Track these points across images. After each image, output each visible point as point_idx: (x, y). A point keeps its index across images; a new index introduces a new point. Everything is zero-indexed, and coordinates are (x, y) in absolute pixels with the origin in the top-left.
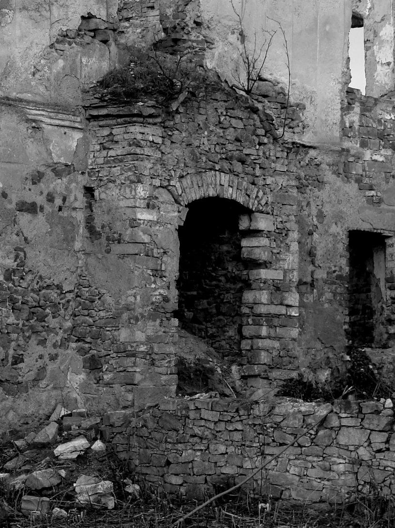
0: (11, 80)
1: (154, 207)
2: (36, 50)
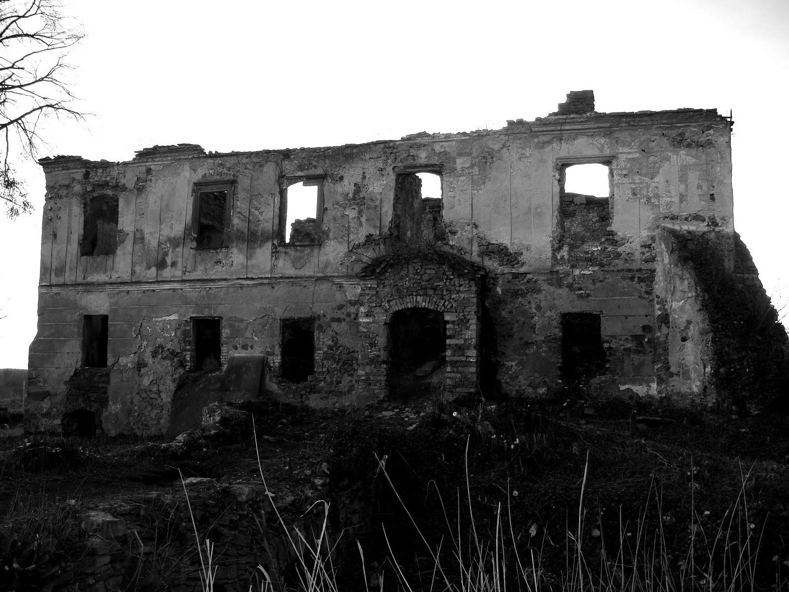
0: (329, 269)
1: (370, 316)
2: (341, 255)
